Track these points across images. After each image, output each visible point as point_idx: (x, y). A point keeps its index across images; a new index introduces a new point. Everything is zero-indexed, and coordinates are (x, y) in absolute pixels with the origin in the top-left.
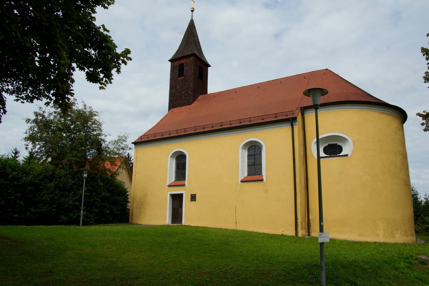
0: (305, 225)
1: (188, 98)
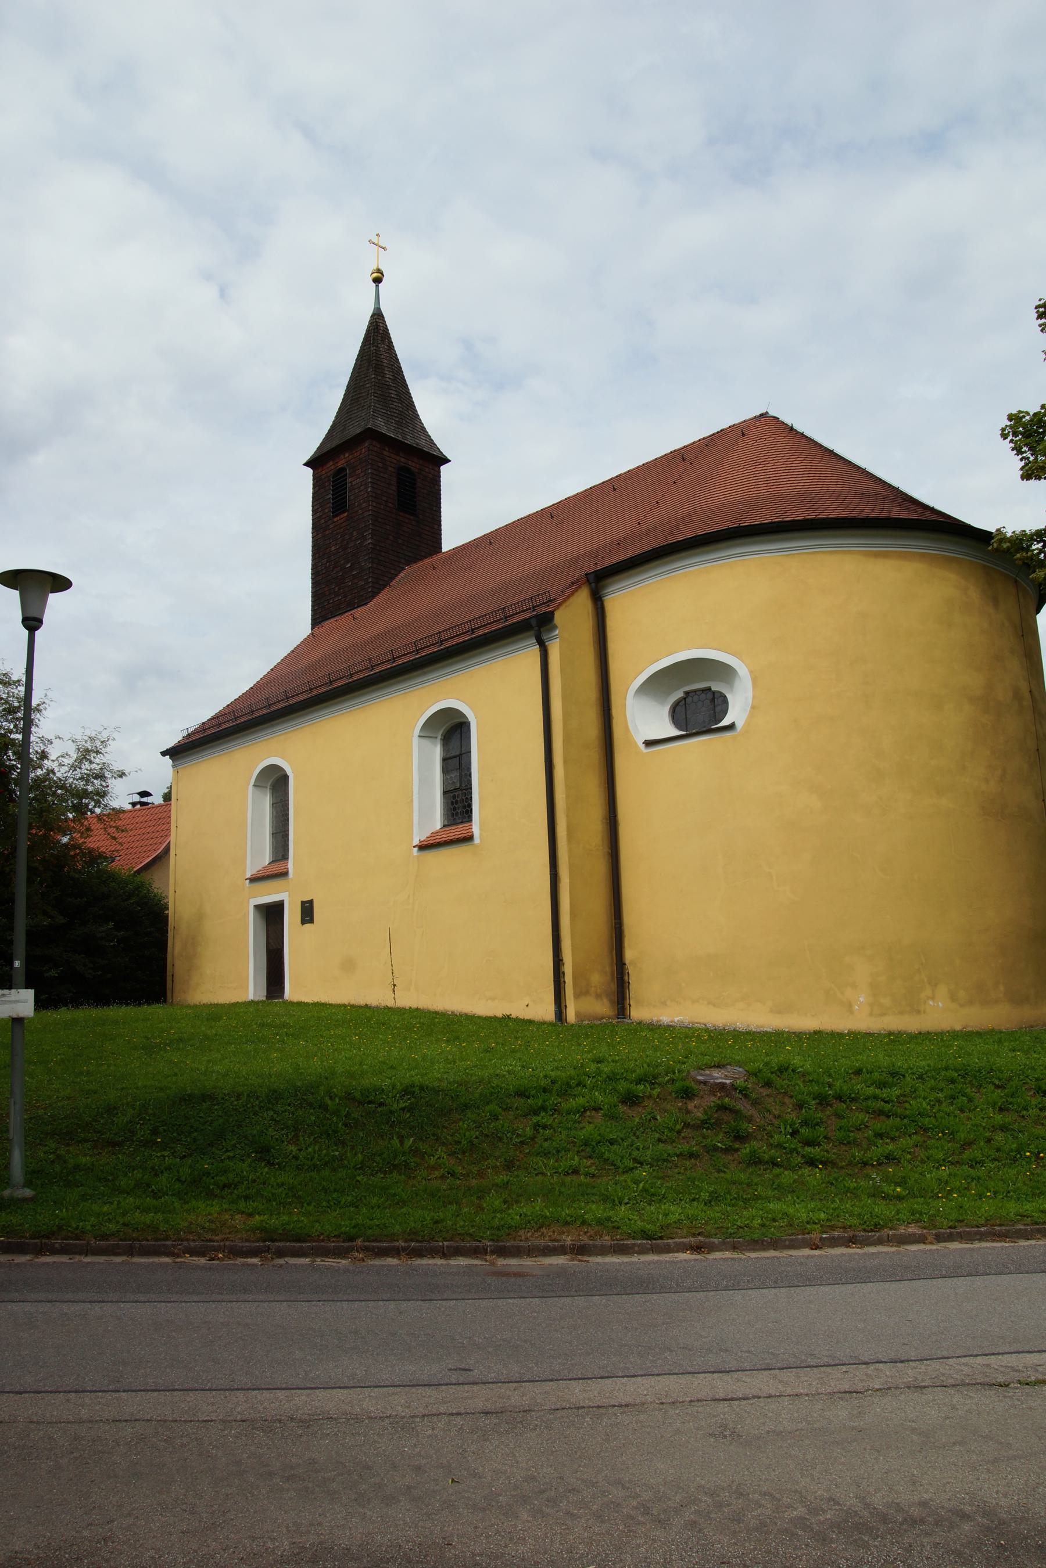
0: (600, 978)
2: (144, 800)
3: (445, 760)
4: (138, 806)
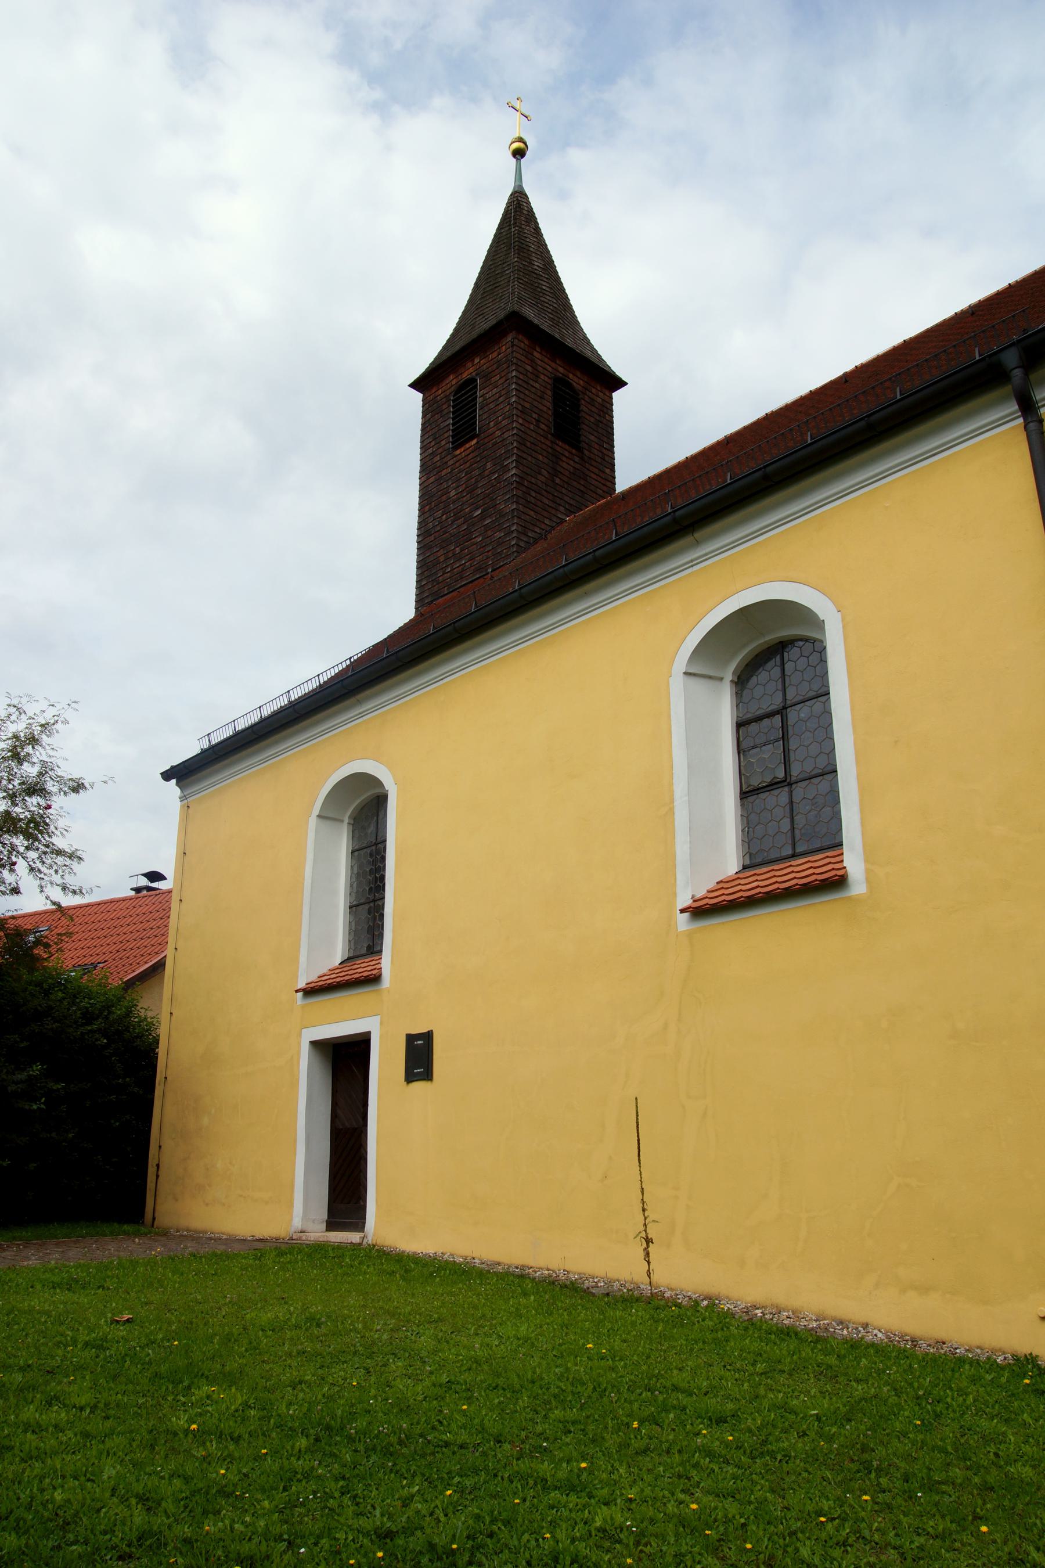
1: (498, 535)
2: (155, 885)
3: (740, 725)
4: (145, 892)
